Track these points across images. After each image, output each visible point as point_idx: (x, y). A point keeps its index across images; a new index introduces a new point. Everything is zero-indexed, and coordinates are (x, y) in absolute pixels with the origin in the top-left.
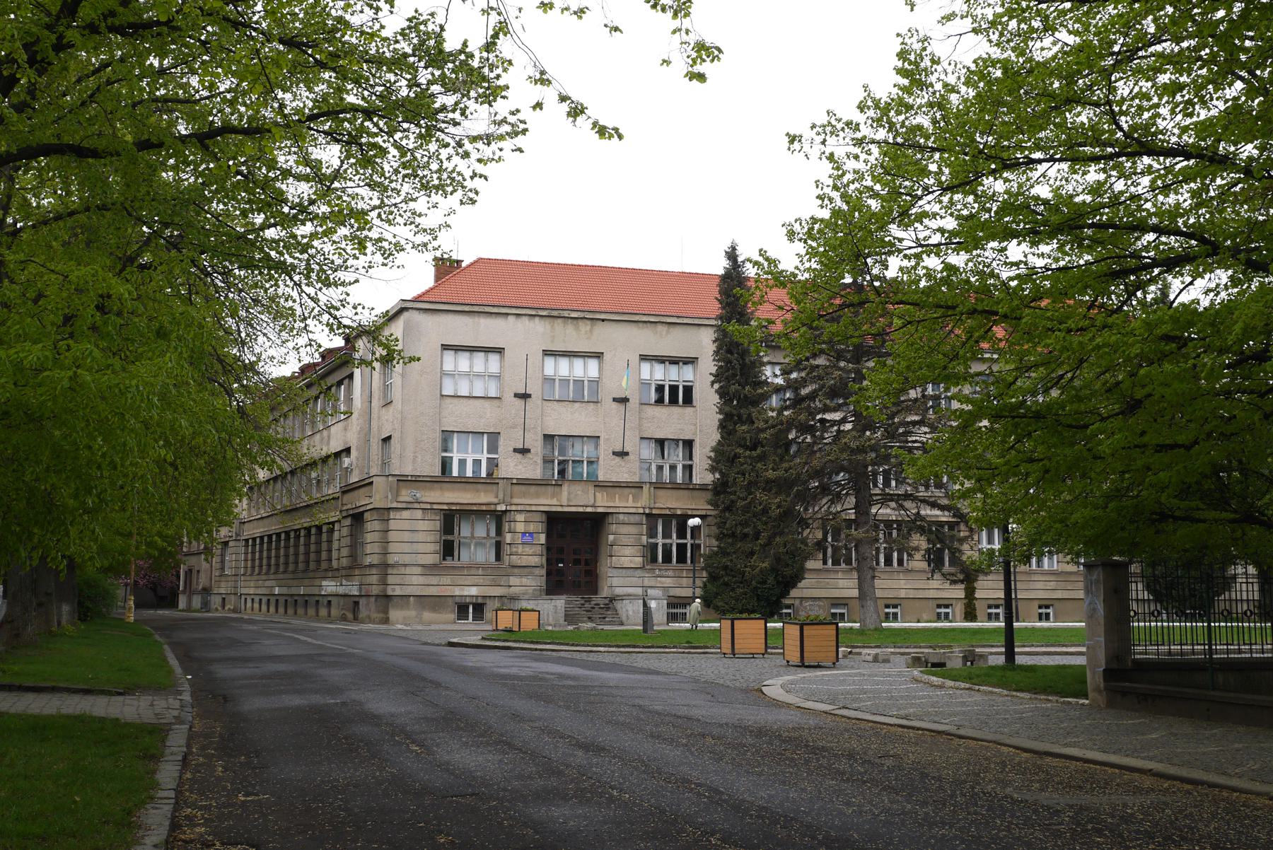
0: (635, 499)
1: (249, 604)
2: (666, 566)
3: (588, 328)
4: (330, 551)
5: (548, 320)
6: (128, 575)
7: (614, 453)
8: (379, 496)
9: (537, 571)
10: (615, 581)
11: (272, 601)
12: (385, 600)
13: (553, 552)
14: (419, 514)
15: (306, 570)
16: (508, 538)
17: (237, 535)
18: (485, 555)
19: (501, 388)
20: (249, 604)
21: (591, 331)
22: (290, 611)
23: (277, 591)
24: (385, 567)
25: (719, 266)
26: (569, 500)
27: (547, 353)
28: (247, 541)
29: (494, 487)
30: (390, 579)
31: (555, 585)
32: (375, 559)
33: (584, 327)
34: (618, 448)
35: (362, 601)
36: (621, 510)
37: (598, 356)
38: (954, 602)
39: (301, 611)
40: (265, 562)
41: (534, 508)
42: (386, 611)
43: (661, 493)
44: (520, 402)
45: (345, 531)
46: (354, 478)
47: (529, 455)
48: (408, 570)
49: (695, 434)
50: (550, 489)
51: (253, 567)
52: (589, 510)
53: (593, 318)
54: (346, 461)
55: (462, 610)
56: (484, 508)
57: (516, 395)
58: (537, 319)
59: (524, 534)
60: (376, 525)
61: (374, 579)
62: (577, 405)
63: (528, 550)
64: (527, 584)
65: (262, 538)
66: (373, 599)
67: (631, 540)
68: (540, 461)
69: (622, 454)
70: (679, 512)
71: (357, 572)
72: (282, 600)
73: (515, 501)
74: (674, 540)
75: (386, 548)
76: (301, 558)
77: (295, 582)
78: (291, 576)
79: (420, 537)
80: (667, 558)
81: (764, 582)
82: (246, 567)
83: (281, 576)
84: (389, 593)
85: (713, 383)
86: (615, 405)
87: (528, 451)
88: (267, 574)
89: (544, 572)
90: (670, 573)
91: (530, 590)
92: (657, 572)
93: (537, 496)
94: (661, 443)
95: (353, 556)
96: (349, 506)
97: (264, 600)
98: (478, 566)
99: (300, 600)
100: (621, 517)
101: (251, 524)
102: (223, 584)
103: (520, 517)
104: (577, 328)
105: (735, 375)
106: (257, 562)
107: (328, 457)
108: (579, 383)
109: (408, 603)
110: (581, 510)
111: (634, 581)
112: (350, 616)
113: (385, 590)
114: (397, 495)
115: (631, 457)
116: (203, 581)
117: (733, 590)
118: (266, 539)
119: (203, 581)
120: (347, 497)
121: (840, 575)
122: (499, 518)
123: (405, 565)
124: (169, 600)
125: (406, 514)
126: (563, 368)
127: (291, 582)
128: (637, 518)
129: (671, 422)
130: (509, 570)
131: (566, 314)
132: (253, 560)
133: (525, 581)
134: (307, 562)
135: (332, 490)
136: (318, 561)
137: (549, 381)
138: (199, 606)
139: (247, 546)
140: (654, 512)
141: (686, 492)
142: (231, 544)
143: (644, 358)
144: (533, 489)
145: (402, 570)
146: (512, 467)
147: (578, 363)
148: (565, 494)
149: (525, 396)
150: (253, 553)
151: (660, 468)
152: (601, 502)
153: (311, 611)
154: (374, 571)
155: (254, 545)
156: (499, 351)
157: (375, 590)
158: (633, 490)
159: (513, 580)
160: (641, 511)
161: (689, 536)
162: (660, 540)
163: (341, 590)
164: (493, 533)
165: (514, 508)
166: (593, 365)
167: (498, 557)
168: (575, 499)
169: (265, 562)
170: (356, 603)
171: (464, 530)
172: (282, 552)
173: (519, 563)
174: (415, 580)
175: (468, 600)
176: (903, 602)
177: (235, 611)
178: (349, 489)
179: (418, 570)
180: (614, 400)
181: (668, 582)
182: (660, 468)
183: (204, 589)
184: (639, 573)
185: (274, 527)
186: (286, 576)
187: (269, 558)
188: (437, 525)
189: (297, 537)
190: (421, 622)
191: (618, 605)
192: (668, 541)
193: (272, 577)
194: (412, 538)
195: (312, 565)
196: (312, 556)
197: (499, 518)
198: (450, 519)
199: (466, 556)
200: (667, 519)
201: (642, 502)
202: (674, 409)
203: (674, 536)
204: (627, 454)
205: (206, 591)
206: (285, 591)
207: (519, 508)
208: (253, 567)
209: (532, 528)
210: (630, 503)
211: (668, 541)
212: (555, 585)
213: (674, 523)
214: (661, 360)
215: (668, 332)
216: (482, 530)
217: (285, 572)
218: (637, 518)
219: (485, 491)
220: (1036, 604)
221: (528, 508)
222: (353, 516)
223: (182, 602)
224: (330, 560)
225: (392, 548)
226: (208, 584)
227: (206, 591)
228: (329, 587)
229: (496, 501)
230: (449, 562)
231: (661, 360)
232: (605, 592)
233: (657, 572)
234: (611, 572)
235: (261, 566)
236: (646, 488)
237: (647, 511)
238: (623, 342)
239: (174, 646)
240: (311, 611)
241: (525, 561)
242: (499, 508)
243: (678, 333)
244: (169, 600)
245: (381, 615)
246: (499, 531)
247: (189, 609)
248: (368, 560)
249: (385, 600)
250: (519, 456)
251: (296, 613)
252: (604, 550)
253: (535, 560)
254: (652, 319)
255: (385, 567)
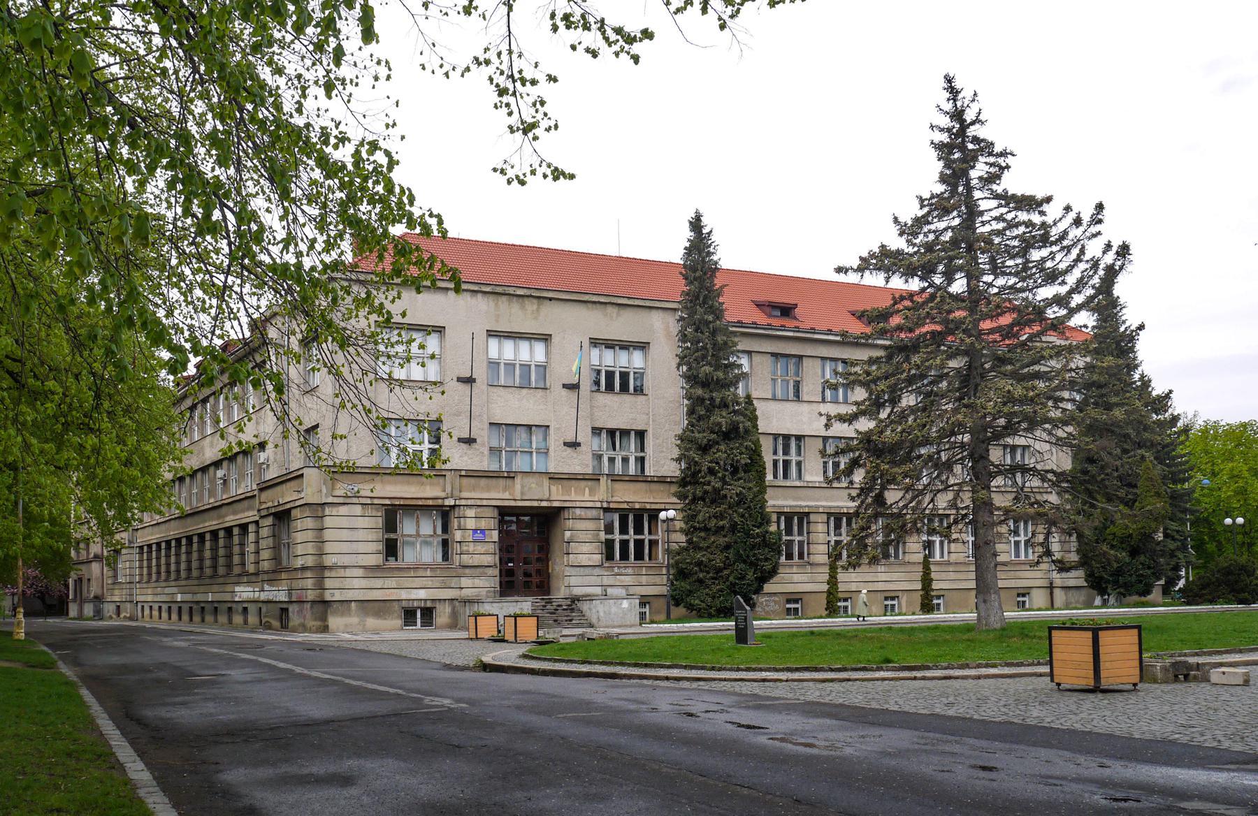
0: (592, 492)
1: (147, 612)
2: (623, 563)
3: (535, 307)
4: (242, 554)
5: (491, 297)
6: (15, 585)
7: (565, 444)
8: (313, 487)
9: (490, 571)
10: (573, 581)
11: (172, 607)
12: (323, 606)
13: (507, 548)
14: (358, 510)
15: (215, 575)
16: (458, 535)
17: (130, 542)
18: (431, 554)
19: (442, 371)
20: (147, 612)
21: (538, 310)
22: (197, 618)
23: (179, 598)
24: (320, 570)
25: (671, 247)
26: (522, 493)
27: (491, 334)
28: (141, 548)
29: (441, 480)
30: (328, 583)
31: (509, 586)
32: (310, 561)
33: (531, 306)
34: (571, 439)
35: (293, 609)
36: (578, 504)
37: (546, 338)
38: (900, 594)
39: (209, 618)
40: (163, 568)
41: (485, 503)
42: (324, 618)
43: (618, 486)
44: (465, 388)
45: (264, 532)
46: (272, 474)
47: (474, 445)
48: (348, 573)
49: (647, 424)
50: (501, 481)
51: (150, 574)
52: (544, 504)
53: (540, 297)
54: (262, 456)
55: (409, 615)
56: (430, 503)
57: (460, 380)
58: (479, 295)
59: (475, 531)
60: (310, 523)
61: (309, 583)
62: (525, 391)
63: (480, 548)
64: (482, 585)
65: (158, 544)
66: (309, 605)
67: (589, 537)
68: (486, 452)
69: (574, 445)
70: (637, 506)
71: (284, 576)
72: (185, 608)
73: (464, 495)
74: (631, 536)
75: (320, 549)
76: (208, 563)
77: (202, 589)
78: (196, 582)
79: (361, 535)
80: (625, 556)
81: (743, 578)
82: (141, 575)
83: (183, 583)
84: (328, 597)
85: (679, 365)
86: (565, 392)
87: (474, 441)
88: (166, 580)
89: (497, 572)
90: (630, 571)
91: (483, 592)
92: (616, 570)
93: (488, 489)
94: (612, 433)
95: (276, 558)
96: (270, 504)
97: (165, 607)
98: (425, 567)
99: (207, 606)
100: (578, 511)
101: (146, 531)
102: (116, 592)
103: (471, 513)
104: (523, 307)
105: (704, 357)
106: (154, 569)
107: (195, 472)
108: (526, 367)
109: (349, 609)
110: (535, 504)
111: (593, 580)
112: (276, 624)
113: (322, 595)
114: (333, 489)
115: (583, 448)
116: (94, 590)
117: (708, 587)
118: (163, 545)
119: (94, 590)
120: (264, 495)
121: (795, 570)
122: (445, 514)
123: (345, 567)
124: (59, 608)
125: (343, 510)
126: (509, 351)
127: (195, 589)
128: (594, 513)
129: (619, 411)
130: (460, 571)
131: (511, 290)
132: (149, 567)
133: (477, 582)
134: (215, 567)
135: (248, 485)
136: (229, 566)
137: (494, 365)
138: (91, 614)
139: (141, 553)
140: (612, 506)
141: (643, 484)
142: (124, 551)
143: (595, 342)
144: (483, 482)
145: (341, 573)
146: (457, 457)
147: (524, 346)
148: (518, 487)
149: (469, 381)
150: (149, 560)
151: (612, 460)
152: (556, 495)
153: (223, 619)
154: (309, 574)
155: (150, 552)
156: (440, 330)
157: (311, 595)
158: (590, 483)
159: (465, 582)
160: (599, 505)
161: (646, 531)
162: (617, 537)
163: (263, 596)
164: (439, 531)
165: (463, 502)
166: (539, 348)
167: (445, 557)
168: (531, 493)
169: (163, 568)
170: (285, 611)
171: (407, 527)
172: (183, 557)
173: (471, 563)
174: (357, 583)
175: (416, 604)
176: (853, 595)
177: (131, 619)
178: (265, 487)
179: (360, 572)
180: (565, 386)
181: (627, 580)
182: (612, 460)
183: (96, 597)
184: (597, 571)
185: (173, 531)
186: (190, 582)
187: (168, 564)
188: (380, 522)
189: (159, 549)
190: (365, 630)
191: (585, 606)
192: (625, 537)
193: (173, 583)
194: (350, 537)
195: (221, 571)
196: (221, 561)
197: (445, 514)
198: (392, 514)
199: (409, 555)
200: (639, 515)
201: (602, 493)
202: (625, 397)
203: (631, 531)
204: (579, 445)
205: (98, 599)
206: (188, 597)
207: (469, 502)
208: (150, 574)
209: (483, 524)
210: (587, 497)
211: (625, 537)
212: (509, 586)
213: (631, 517)
214: (610, 345)
215: (618, 314)
216: (428, 526)
217: (188, 578)
218: (594, 513)
219: (431, 484)
220: (1015, 592)
221: (479, 503)
222: (275, 515)
223: (73, 610)
224: (243, 564)
225: (329, 548)
226: (99, 592)
227: (98, 599)
228: (244, 592)
229: (443, 495)
230: (392, 563)
231: (610, 345)
232: (560, 593)
233: (616, 570)
234: (568, 571)
235: (159, 573)
236: (603, 480)
237: (605, 505)
238: (573, 326)
239: (96, 682)
240: (223, 619)
241: (476, 560)
242: (447, 502)
243: (628, 315)
244: (59, 608)
245: (319, 623)
246: (445, 529)
247: (80, 617)
248: (299, 562)
249: (323, 606)
250: (464, 446)
251: (203, 621)
252: (557, 547)
253: (488, 560)
254: (602, 299)
255: (320, 570)
